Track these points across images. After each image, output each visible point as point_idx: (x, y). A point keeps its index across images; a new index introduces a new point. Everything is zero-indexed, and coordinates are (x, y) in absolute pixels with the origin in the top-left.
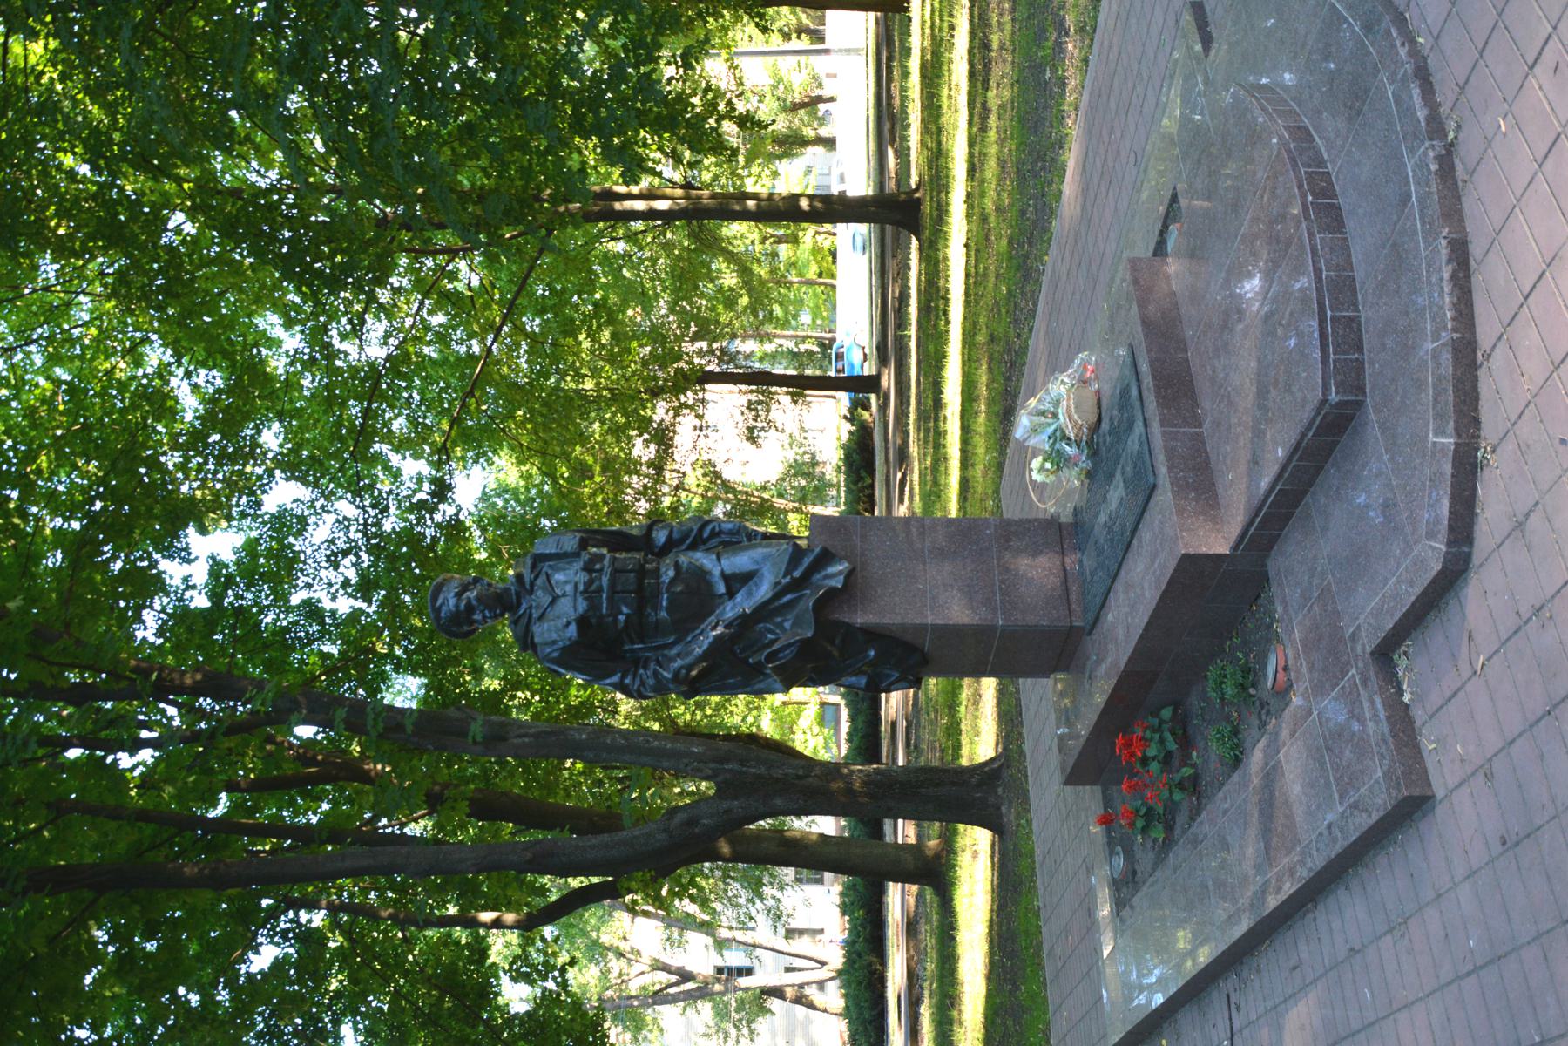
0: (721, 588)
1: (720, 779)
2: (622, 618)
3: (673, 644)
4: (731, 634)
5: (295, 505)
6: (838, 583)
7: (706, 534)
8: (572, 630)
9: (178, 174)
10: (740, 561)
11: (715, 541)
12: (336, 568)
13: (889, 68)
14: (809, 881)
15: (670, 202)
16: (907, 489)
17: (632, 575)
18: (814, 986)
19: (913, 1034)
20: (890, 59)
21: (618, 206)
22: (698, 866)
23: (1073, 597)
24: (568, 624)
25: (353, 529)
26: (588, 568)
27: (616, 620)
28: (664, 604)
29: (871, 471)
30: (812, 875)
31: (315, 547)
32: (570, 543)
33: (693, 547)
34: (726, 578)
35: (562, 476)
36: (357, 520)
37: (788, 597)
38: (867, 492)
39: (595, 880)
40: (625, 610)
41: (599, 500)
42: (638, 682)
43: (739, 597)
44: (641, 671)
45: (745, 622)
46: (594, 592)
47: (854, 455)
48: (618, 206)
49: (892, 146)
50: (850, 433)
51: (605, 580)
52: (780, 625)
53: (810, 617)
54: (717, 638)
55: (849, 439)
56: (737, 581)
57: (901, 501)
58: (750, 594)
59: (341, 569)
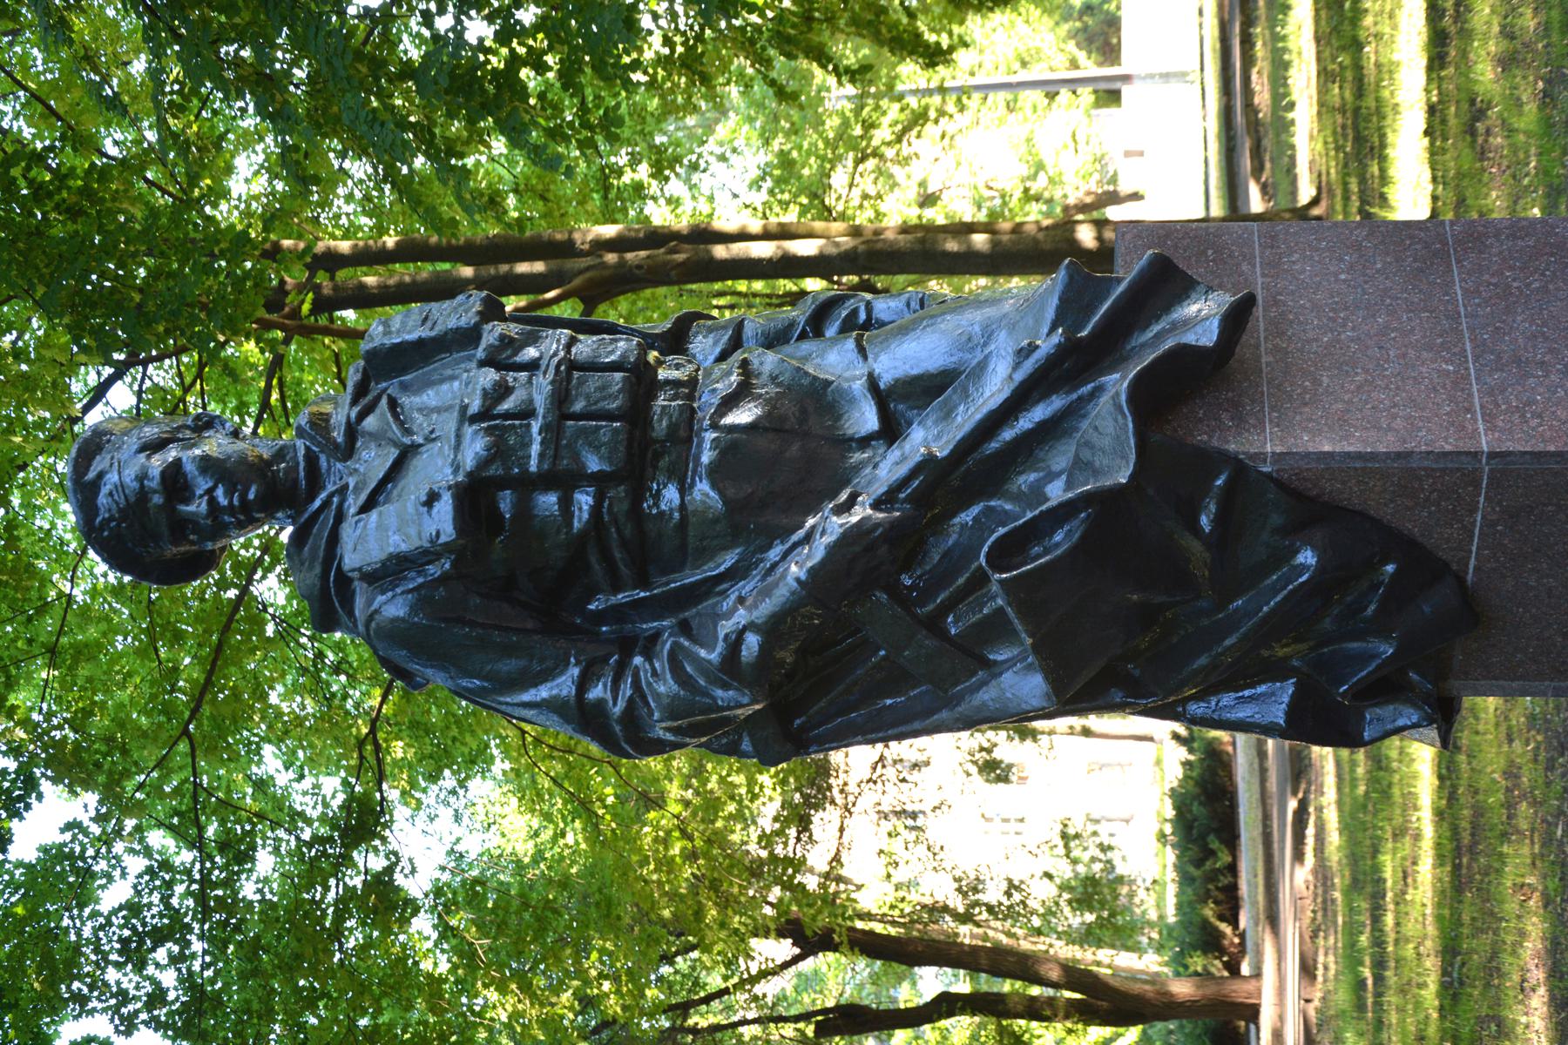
0: (867, 418)
4: (893, 525)
5: (68, 836)
6: (1207, 336)
12: (140, 966)
13: (1247, 41)
15: (821, 242)
16: (1310, 831)
17: (618, 376)
18: (1230, 859)
20: (1248, 22)
21: (720, 251)
24: (432, 498)
25: (179, 889)
28: (706, 458)
29: (1230, 837)
31: (102, 920)
35: (602, 800)
36: (188, 872)
38: (1225, 881)
41: (676, 849)
42: (626, 690)
44: (638, 660)
46: (507, 415)
47: (1196, 808)
48: (720, 251)
49: (1258, 180)
50: (1187, 764)
54: (852, 536)
55: (1186, 777)
57: (1299, 856)
59: (150, 970)
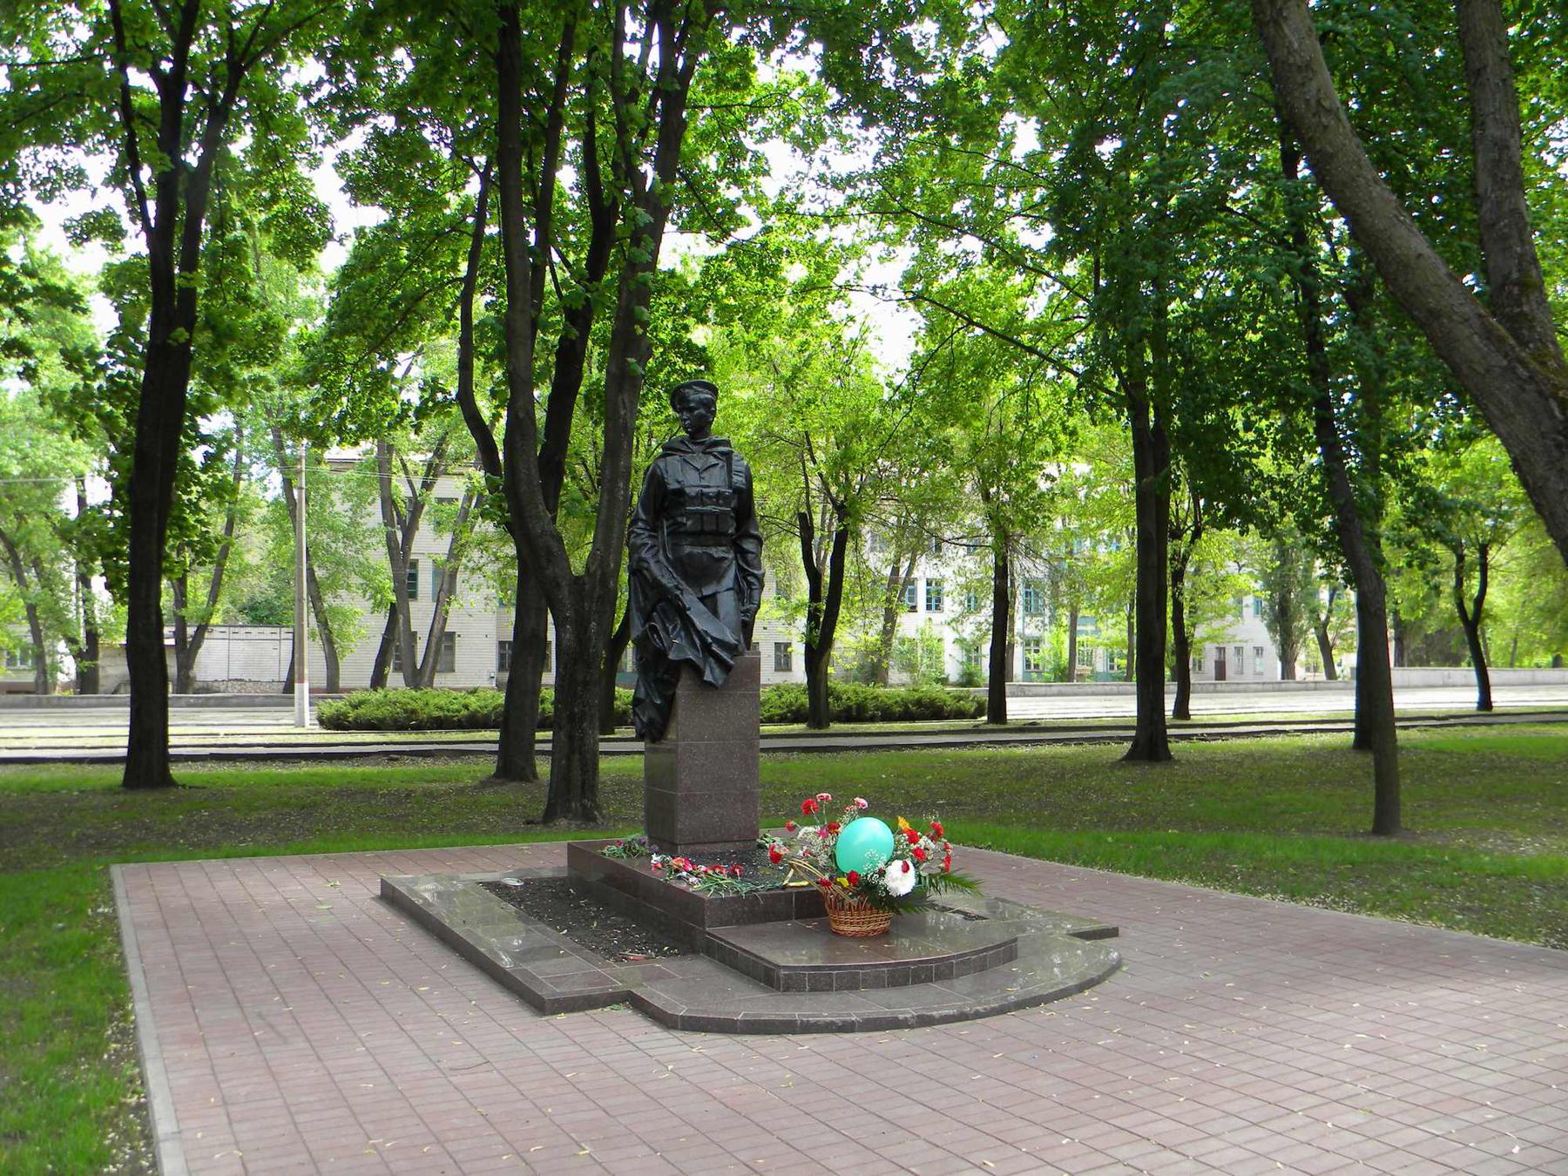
0: (707, 591)
1: (586, 579)
2: (684, 520)
6: (708, 677)
8: (673, 486)
10: (727, 601)
14: (502, 657)
23: (698, 847)
27: (682, 515)
30: (507, 661)
33: (740, 568)
37: (698, 642)
39: (501, 456)
40: (689, 523)
42: (639, 531)
45: (682, 612)
52: (678, 635)
53: (682, 656)
56: (710, 602)
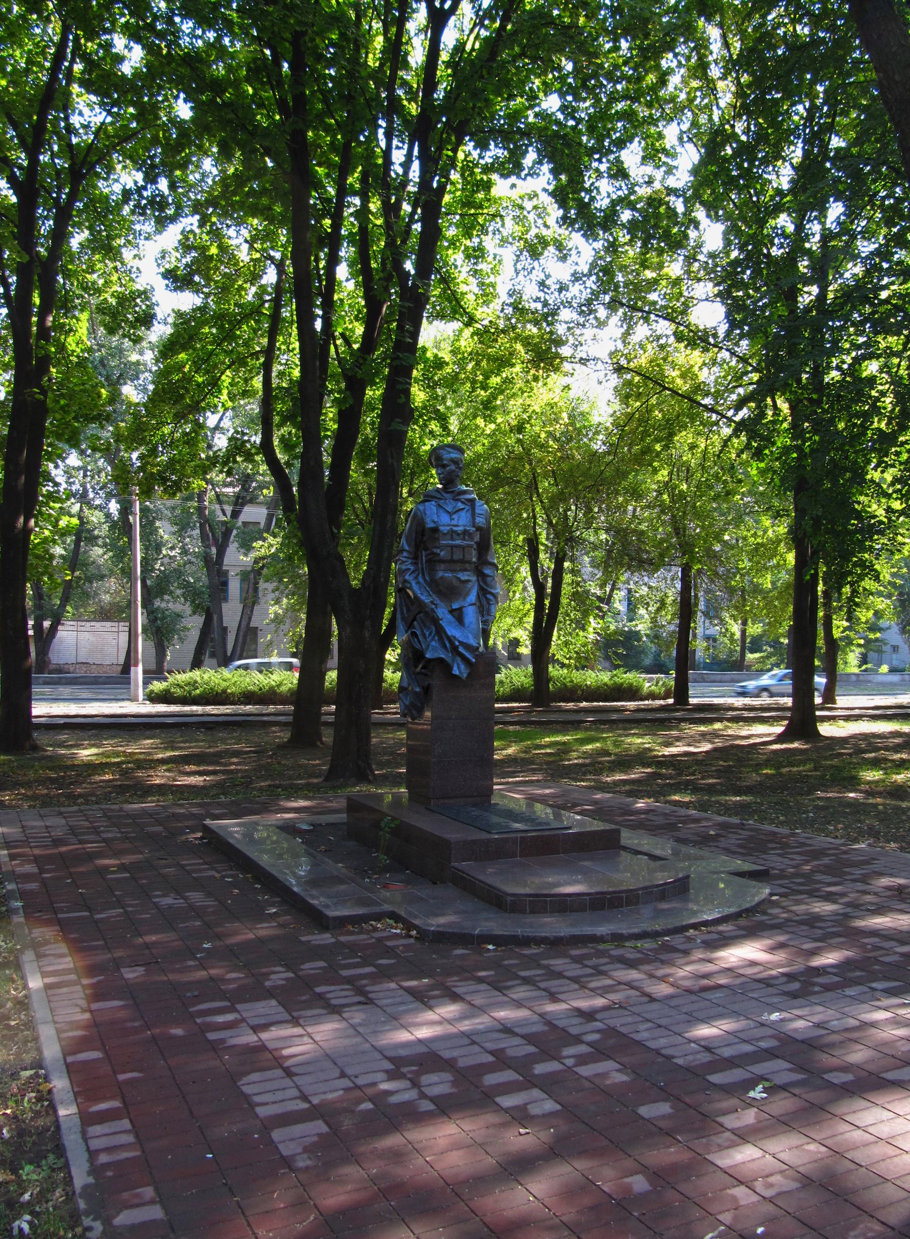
0: (455, 606)
3: (425, 580)
6: (456, 671)
7: (489, 596)
9: (187, 841)
10: (471, 615)
11: (484, 602)
19: (901, 765)
22: (305, 610)
26: (465, 532)
32: (480, 521)
34: (460, 609)
43: (449, 616)
51: (458, 542)
56: (458, 616)
58: (450, 623)
